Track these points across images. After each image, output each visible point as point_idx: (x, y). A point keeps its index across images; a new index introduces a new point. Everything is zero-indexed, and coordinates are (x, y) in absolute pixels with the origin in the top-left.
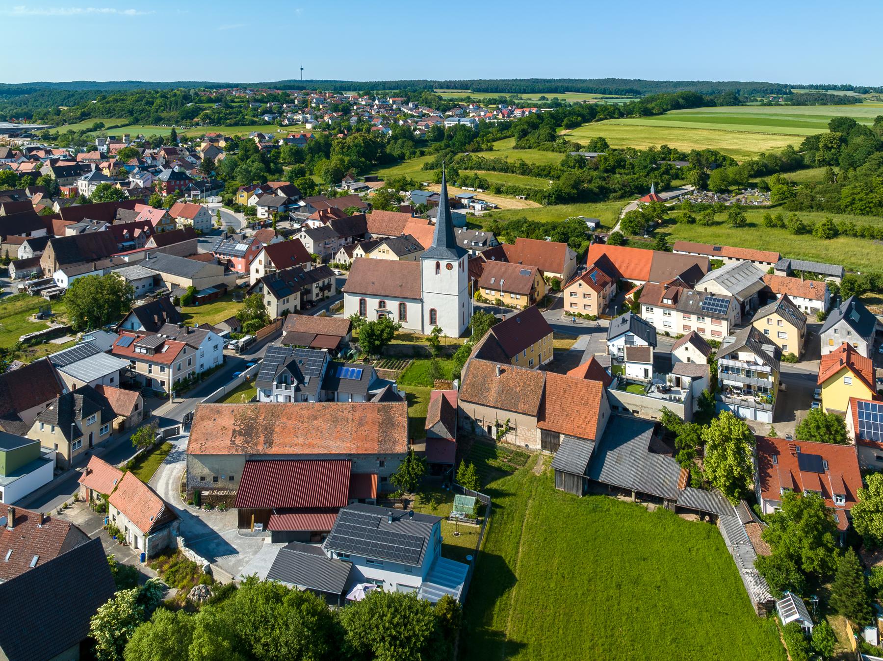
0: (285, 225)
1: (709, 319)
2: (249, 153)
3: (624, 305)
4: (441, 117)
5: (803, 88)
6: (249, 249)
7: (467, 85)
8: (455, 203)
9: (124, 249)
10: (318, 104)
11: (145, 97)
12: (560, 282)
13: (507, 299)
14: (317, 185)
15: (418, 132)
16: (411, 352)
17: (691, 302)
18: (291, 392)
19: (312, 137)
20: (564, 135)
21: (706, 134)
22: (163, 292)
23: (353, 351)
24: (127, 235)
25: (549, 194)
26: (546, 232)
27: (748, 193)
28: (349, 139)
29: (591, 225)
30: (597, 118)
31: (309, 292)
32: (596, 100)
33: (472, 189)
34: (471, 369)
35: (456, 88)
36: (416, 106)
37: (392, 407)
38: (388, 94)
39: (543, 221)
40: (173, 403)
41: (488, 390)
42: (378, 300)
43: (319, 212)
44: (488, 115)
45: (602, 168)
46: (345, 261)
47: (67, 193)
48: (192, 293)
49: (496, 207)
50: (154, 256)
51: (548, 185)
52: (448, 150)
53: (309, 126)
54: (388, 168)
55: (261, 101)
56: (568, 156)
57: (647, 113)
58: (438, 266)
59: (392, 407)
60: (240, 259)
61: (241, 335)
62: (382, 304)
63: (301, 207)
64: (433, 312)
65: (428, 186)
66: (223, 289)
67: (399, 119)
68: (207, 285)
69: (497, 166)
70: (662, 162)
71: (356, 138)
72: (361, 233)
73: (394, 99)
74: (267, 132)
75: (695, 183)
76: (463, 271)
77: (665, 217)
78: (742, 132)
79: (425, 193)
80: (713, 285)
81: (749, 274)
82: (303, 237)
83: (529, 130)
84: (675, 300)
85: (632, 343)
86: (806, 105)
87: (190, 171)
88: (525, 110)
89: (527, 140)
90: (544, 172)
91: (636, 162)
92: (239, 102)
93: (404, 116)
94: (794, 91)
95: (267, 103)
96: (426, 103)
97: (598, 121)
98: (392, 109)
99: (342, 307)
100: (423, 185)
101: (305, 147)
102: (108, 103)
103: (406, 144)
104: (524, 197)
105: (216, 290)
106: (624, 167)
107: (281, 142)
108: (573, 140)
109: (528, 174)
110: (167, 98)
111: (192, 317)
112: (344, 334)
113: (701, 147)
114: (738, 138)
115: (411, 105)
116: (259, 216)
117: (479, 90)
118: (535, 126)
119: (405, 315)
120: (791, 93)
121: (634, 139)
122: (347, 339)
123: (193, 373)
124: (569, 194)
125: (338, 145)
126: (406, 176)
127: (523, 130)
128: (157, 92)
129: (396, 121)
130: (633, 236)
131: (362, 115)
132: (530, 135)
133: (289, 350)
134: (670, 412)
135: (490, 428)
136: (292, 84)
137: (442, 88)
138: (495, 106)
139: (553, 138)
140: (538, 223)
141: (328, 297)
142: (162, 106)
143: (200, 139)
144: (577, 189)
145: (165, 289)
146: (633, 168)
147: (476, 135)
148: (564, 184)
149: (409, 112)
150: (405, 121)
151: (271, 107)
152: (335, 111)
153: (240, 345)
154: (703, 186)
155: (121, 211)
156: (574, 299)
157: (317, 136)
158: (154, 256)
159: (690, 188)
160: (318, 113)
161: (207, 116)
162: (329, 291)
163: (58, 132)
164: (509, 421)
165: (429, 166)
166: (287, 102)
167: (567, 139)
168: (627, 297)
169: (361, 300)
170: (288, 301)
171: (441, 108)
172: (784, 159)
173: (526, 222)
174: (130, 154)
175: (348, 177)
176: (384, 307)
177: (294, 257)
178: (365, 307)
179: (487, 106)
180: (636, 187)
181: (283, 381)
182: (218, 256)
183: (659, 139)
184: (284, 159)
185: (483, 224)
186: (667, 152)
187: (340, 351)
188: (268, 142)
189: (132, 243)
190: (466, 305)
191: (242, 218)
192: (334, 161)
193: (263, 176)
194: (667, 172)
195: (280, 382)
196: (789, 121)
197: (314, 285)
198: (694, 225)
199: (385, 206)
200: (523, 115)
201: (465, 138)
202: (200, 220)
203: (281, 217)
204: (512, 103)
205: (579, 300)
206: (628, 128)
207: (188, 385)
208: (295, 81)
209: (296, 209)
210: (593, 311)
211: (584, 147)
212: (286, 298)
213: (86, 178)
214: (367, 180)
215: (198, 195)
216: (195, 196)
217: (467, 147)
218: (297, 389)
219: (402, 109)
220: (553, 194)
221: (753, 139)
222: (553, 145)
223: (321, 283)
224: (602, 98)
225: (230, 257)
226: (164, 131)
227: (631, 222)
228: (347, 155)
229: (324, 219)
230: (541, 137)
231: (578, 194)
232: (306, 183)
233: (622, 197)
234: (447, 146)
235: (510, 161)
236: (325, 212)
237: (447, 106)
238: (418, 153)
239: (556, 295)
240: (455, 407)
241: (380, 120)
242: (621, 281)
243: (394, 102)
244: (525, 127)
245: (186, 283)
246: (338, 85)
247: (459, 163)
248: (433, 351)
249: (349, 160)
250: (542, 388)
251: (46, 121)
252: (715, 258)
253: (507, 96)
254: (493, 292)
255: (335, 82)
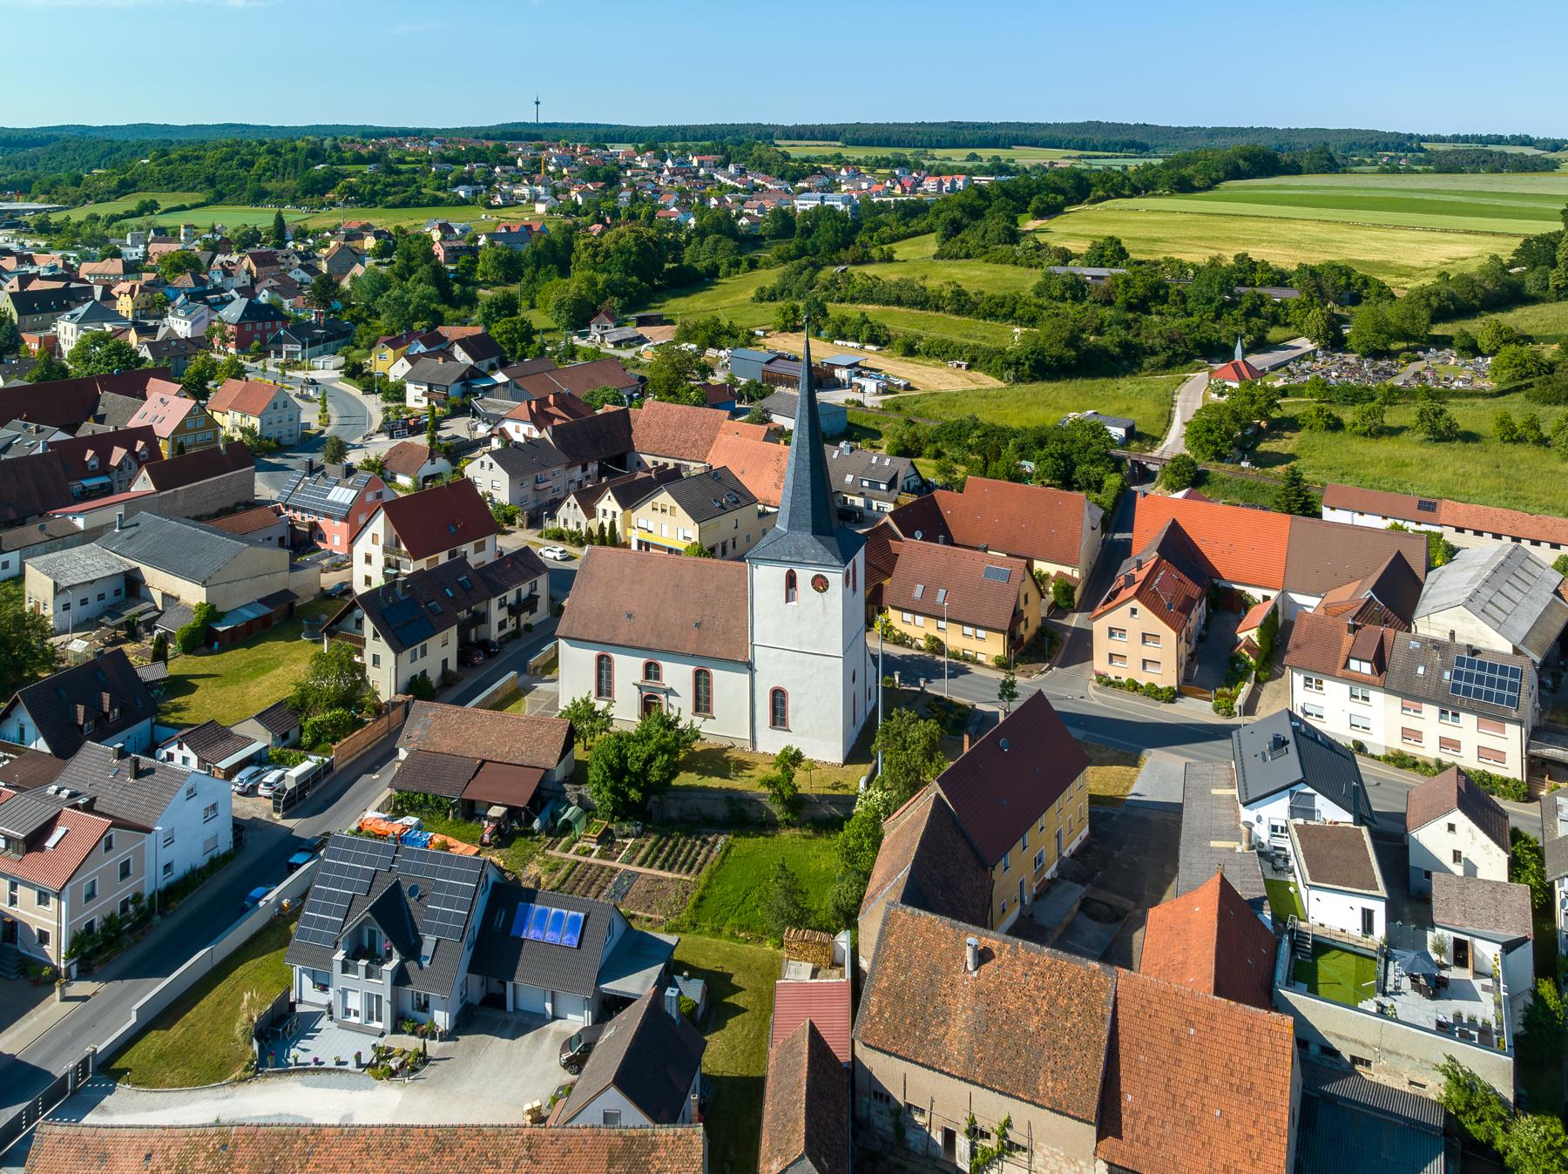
0: (458, 428)
1: (1473, 718)
2: (413, 264)
3: (1237, 658)
4: (787, 192)
5: (1441, 140)
6: (359, 501)
7: (834, 133)
8: (821, 378)
9: (87, 495)
10: (559, 166)
11: (238, 153)
12: (1074, 589)
13: (956, 639)
14: (537, 332)
15: (744, 221)
16: (721, 811)
17: (1421, 670)
18: (382, 986)
19: (543, 231)
20: (1035, 231)
21: (1314, 230)
22: (141, 614)
23: (571, 813)
24: (94, 463)
25: (1018, 359)
26: (1022, 449)
27: (1432, 358)
28: (610, 236)
29: (1118, 432)
30: (1091, 197)
31: (481, 618)
32: (1070, 162)
33: (855, 345)
34: (892, 940)
35: (815, 139)
36: (742, 171)
37: (655, 1146)
38: (689, 148)
39: (1015, 425)
40: (65, 999)
41: (945, 1016)
42: (642, 661)
43: (529, 404)
44: (876, 188)
45: (1119, 301)
46: (578, 525)
47: (35, 347)
48: (204, 622)
49: (908, 387)
50: (133, 521)
51: (1015, 336)
52: (804, 260)
53: (540, 208)
54: (686, 295)
55: (454, 161)
56: (1049, 276)
57: (1184, 187)
58: (791, 581)
59: (655, 1146)
60: (338, 523)
61: (295, 754)
62: (651, 671)
63: (497, 385)
64: (778, 697)
65: (765, 337)
66: (285, 606)
67: (709, 195)
68: (243, 598)
69: (904, 297)
70: (1243, 290)
71: (622, 236)
72: (617, 452)
73: (701, 158)
74: (459, 220)
75: (1318, 337)
76: (855, 589)
77: (1275, 415)
78: (1380, 226)
79: (758, 354)
80: (1462, 619)
81: (1531, 581)
82: (487, 466)
83: (965, 221)
84: (1380, 663)
85: (1310, 813)
86: (1462, 172)
87: (292, 300)
88: (943, 178)
89: (963, 241)
90: (1003, 309)
91: (1191, 290)
92: (412, 163)
93: (720, 189)
94: (1425, 146)
95: (464, 164)
96: (760, 165)
97: (1094, 202)
98: (697, 177)
99: (552, 664)
100: (753, 334)
101: (526, 249)
102: (169, 163)
103: (721, 245)
104: (964, 364)
105: (265, 610)
106: (1164, 300)
107: (482, 241)
108: (1055, 242)
109: (970, 313)
110: (279, 154)
111: (193, 689)
112: (551, 761)
113: (1315, 258)
114: (1376, 239)
115: (732, 169)
116: (410, 403)
117: (856, 143)
118: (976, 213)
119: (708, 701)
120: (1422, 150)
121: (1175, 240)
122: (559, 775)
123: (137, 897)
124: (1059, 359)
125: (586, 249)
126: (720, 314)
127: (953, 221)
128: (262, 143)
129: (704, 200)
130: (1215, 463)
131: (641, 188)
132: (966, 231)
133: (386, 850)
134: (1470, 1075)
135: (949, 1136)
136: (519, 129)
137: (788, 138)
138: (887, 171)
139: (1013, 237)
140: (1003, 430)
141: (528, 627)
142: (269, 170)
143: (332, 232)
144: (1077, 348)
145: (147, 605)
146: (1184, 301)
147: (857, 227)
148: (1048, 337)
149: (729, 182)
150: (721, 200)
151: (471, 172)
152: (591, 181)
153: (290, 785)
154: (1335, 342)
155: (109, 401)
156: (1117, 646)
157: (551, 227)
158: (133, 521)
159: (1305, 344)
160: (559, 184)
161: (351, 190)
162: (533, 610)
163: (68, 218)
164: (1008, 1124)
165: (767, 293)
166: (503, 163)
167: (1042, 238)
168: (1242, 636)
169: (600, 658)
170: (424, 653)
171: (789, 174)
172: (1489, 285)
173: (976, 426)
174: (186, 263)
175: (602, 316)
176: (657, 677)
177: (455, 525)
178: (610, 677)
179: (872, 172)
180: (1198, 345)
181: (362, 951)
182: (290, 513)
183: (1223, 240)
184: (485, 274)
185: (881, 428)
186: (1247, 269)
187: (538, 814)
188: (459, 239)
189: (104, 480)
190: (860, 677)
191: (374, 406)
192: (575, 284)
193: (435, 312)
194: (1253, 312)
195: (355, 954)
196: (1460, 203)
197: (494, 602)
198: (1340, 434)
199: (671, 391)
200: (940, 188)
201: (836, 234)
202: (274, 417)
203: (454, 407)
204: (919, 166)
205: (1129, 646)
206: (1157, 217)
207: (119, 934)
208: (525, 124)
209: (486, 390)
210: (1167, 677)
211: (1078, 256)
212: (418, 647)
213: (73, 316)
214: (642, 322)
215: (297, 353)
216: (290, 354)
217: (842, 254)
218: (400, 978)
219: (716, 176)
220: (1027, 358)
221: (1407, 241)
222: (1014, 251)
223: (511, 596)
224: (1080, 158)
225: (315, 518)
226: (261, 218)
227: (1210, 431)
228: (603, 271)
229: (539, 419)
230: (990, 235)
231: (1078, 358)
232: (515, 330)
233: (1168, 365)
234: (802, 252)
235: (932, 284)
236: (543, 402)
237: (799, 172)
238: (745, 265)
239: (1065, 622)
240: (844, 1057)
241: (674, 198)
242: (1215, 587)
243: (701, 164)
244: (958, 214)
245: (193, 594)
246: (601, 132)
247: (826, 289)
248: (778, 811)
249: (606, 281)
250: (1107, 1026)
251: (55, 197)
252: (1424, 527)
253: (908, 152)
254: (920, 619)
255: (597, 126)
